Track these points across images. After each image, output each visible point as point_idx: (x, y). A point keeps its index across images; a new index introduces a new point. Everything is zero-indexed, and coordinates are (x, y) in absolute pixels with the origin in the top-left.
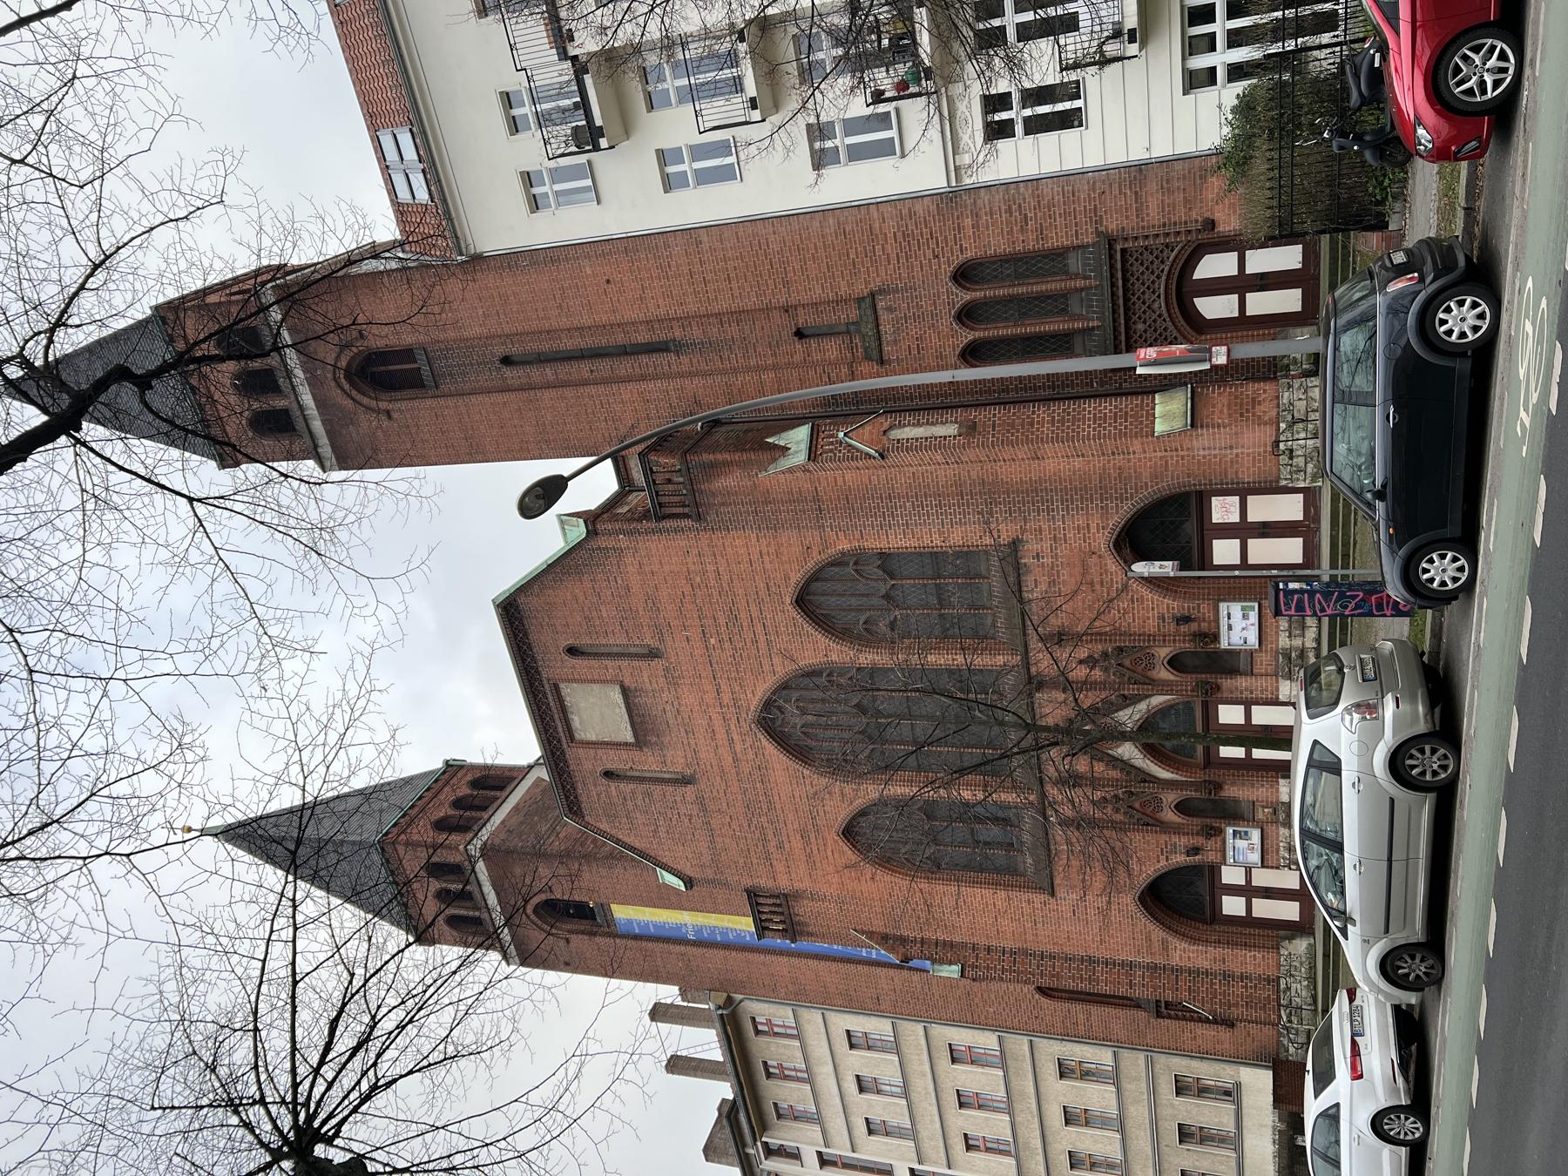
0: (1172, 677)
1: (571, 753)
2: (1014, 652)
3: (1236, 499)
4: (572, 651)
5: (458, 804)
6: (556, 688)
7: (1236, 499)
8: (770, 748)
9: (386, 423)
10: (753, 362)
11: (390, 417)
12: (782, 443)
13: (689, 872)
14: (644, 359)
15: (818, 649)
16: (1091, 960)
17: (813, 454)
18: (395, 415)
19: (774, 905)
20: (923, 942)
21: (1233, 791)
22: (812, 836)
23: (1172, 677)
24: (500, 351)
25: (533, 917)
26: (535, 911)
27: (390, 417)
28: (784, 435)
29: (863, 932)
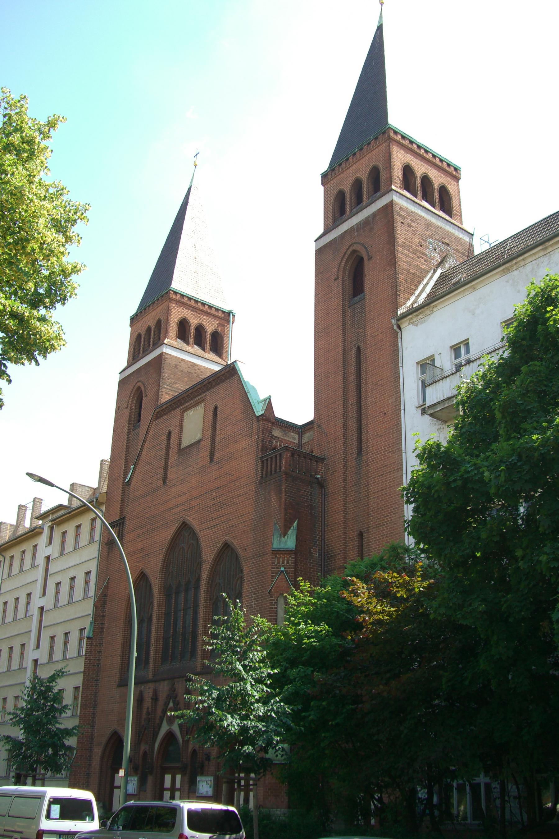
0: (190, 750)
1: (178, 411)
2: (154, 675)
3: (115, 790)
4: (216, 408)
5: (426, 179)
6: (203, 400)
7: (115, 790)
8: (173, 530)
9: (333, 278)
10: (350, 506)
11: (335, 280)
12: (290, 532)
13: (133, 483)
14: (355, 437)
15: (208, 555)
16: (95, 706)
17: (277, 552)
18: (337, 282)
19: (267, 471)
20: (103, 616)
21: (150, 780)
22: (142, 555)
23: (190, 750)
24: (363, 347)
25: (351, 250)
26: (354, 251)
27: (335, 280)
28: (295, 532)
29: (107, 583)
